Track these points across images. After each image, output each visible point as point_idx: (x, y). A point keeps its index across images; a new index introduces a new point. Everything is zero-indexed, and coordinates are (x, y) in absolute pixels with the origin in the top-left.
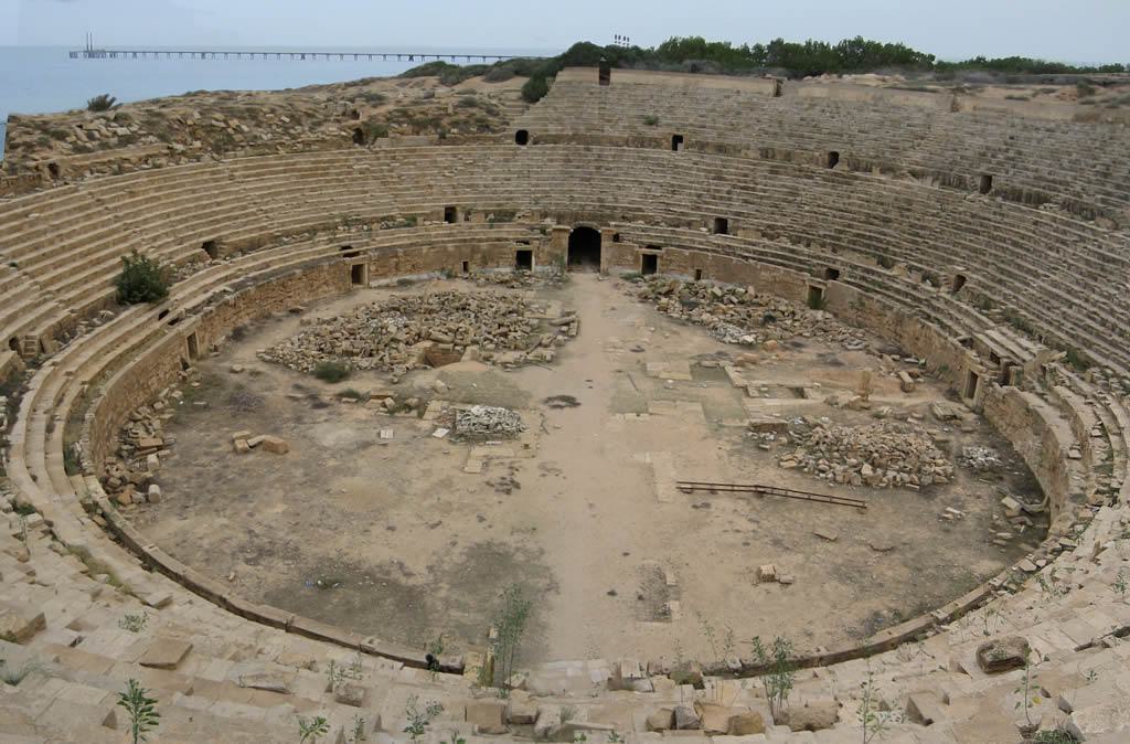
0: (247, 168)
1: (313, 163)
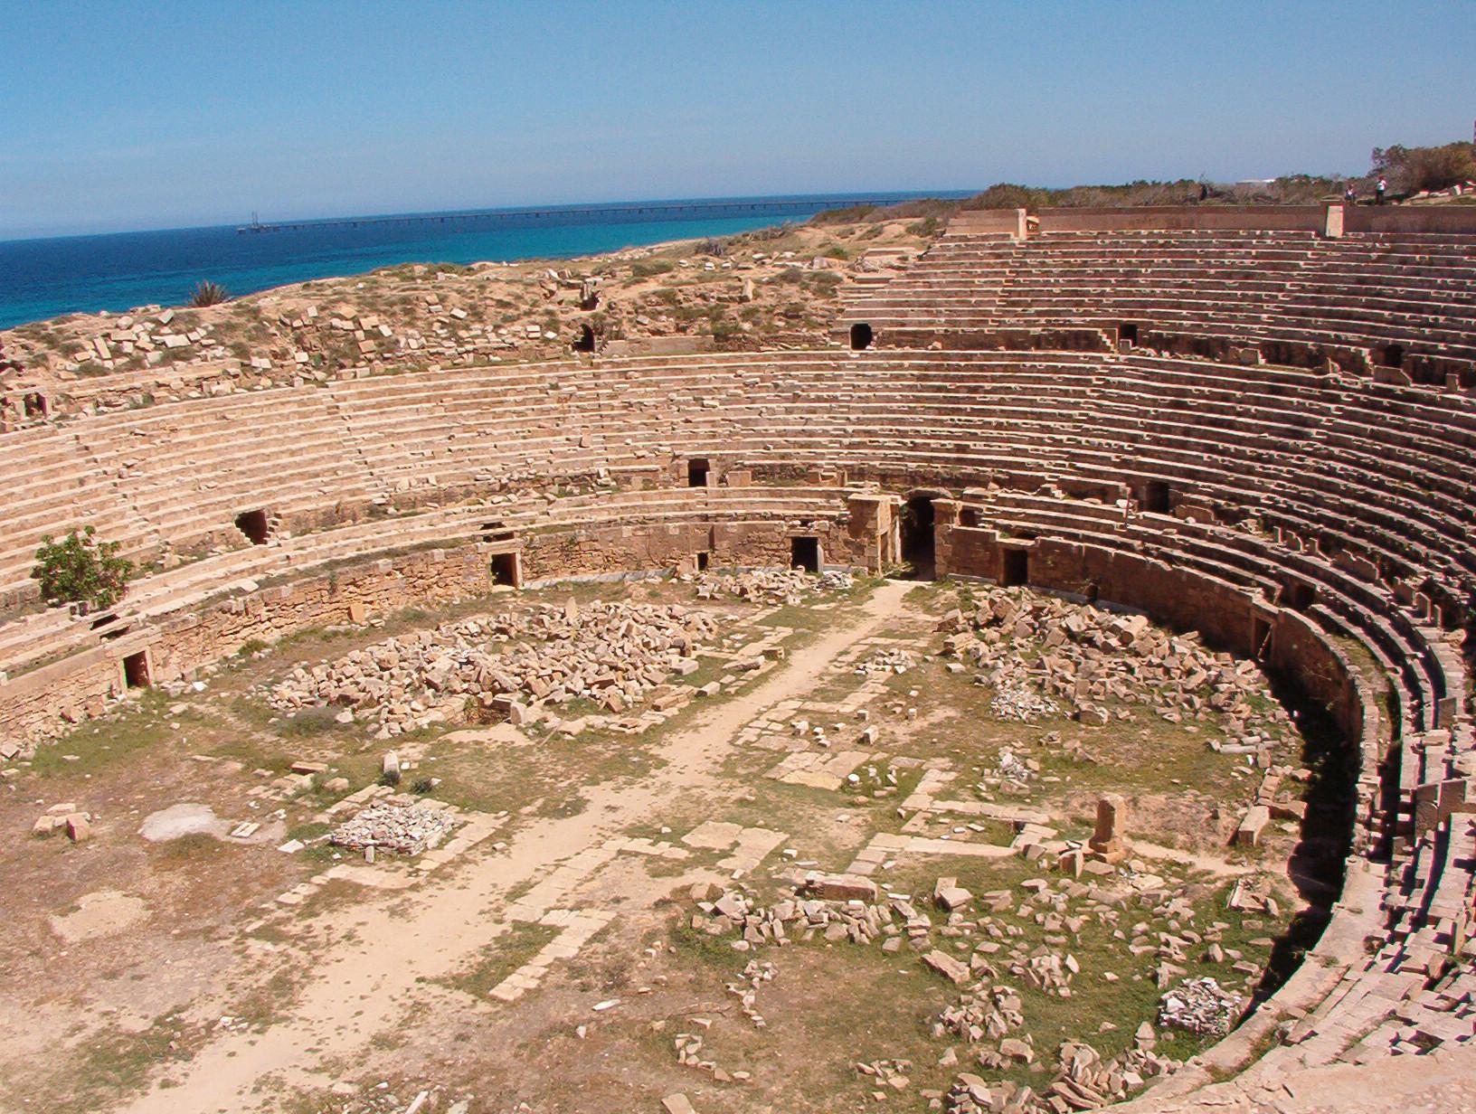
0: (361, 395)
1: (483, 385)
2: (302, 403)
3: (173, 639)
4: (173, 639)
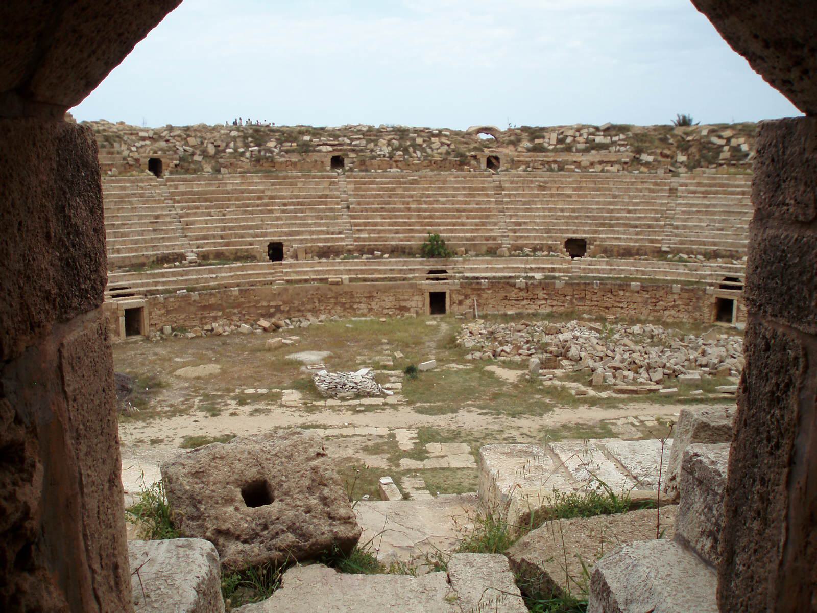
2: (656, 184)
3: (469, 291)
4: (469, 291)
